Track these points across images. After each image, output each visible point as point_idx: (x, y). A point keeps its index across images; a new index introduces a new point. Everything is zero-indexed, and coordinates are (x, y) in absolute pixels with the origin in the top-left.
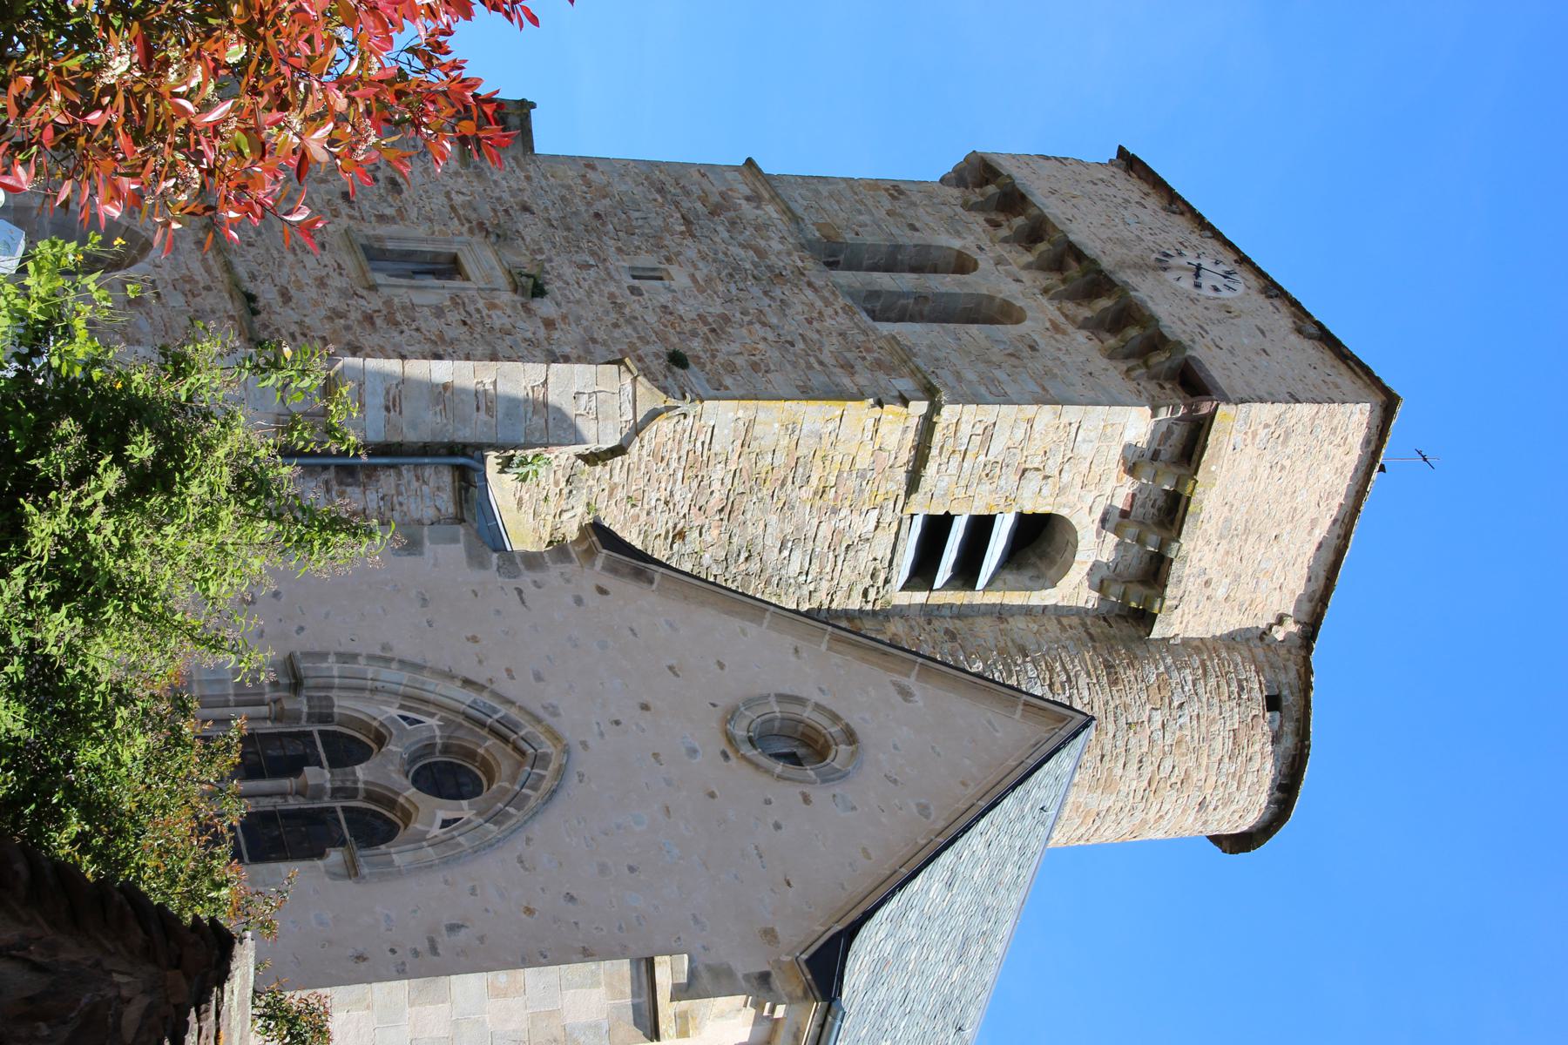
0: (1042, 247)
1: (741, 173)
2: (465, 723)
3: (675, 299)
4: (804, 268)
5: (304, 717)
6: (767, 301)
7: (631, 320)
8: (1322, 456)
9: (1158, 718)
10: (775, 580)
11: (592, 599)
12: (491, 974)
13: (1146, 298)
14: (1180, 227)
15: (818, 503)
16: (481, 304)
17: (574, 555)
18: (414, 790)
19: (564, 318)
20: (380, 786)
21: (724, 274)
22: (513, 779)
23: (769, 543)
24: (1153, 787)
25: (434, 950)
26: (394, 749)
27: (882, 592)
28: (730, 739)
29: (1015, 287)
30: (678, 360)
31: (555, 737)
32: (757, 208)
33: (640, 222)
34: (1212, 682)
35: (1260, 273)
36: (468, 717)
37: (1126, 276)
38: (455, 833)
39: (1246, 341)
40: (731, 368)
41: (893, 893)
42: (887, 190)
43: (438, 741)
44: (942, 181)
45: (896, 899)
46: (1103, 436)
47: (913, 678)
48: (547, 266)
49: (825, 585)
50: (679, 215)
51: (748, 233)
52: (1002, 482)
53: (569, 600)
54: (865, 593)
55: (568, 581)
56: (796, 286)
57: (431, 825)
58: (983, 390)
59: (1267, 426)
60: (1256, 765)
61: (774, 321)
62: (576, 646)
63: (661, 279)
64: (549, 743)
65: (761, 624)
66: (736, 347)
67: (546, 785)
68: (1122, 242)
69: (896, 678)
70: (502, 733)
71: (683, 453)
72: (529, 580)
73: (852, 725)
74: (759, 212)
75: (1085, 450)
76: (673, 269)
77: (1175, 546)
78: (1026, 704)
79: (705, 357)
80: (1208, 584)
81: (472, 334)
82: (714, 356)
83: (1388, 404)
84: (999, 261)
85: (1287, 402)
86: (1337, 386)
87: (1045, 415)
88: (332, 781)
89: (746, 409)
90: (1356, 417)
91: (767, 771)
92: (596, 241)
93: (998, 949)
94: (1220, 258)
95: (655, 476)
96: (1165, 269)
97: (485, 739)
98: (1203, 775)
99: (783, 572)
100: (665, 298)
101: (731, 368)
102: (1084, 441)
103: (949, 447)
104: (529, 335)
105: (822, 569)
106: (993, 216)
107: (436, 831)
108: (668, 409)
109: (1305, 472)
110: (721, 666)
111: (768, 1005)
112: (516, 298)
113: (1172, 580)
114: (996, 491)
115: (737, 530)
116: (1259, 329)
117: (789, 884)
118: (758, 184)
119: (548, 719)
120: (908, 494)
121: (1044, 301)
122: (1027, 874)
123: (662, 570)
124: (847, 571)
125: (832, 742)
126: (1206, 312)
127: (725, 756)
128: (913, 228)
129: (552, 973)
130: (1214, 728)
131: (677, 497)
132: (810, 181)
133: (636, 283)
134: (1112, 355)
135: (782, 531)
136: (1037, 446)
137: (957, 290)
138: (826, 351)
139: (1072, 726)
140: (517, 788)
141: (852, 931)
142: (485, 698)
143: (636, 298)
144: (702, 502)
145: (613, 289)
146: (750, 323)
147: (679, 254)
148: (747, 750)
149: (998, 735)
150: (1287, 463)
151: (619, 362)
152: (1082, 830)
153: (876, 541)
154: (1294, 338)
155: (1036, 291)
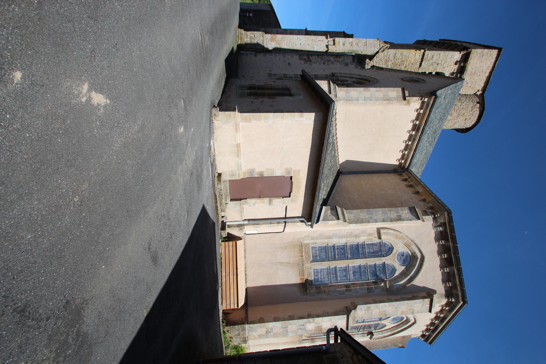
8: (488, 60)
12: (376, 88)
24: (459, 115)
34: (468, 99)
46: (451, 57)
59: (480, 54)
60: (475, 112)
75: (448, 60)
80: (467, 83)
98: (466, 114)
111: (423, 98)
114: (433, 68)
120: (419, 67)
129: (387, 89)
130: (469, 106)
136: (440, 59)
150: (482, 61)
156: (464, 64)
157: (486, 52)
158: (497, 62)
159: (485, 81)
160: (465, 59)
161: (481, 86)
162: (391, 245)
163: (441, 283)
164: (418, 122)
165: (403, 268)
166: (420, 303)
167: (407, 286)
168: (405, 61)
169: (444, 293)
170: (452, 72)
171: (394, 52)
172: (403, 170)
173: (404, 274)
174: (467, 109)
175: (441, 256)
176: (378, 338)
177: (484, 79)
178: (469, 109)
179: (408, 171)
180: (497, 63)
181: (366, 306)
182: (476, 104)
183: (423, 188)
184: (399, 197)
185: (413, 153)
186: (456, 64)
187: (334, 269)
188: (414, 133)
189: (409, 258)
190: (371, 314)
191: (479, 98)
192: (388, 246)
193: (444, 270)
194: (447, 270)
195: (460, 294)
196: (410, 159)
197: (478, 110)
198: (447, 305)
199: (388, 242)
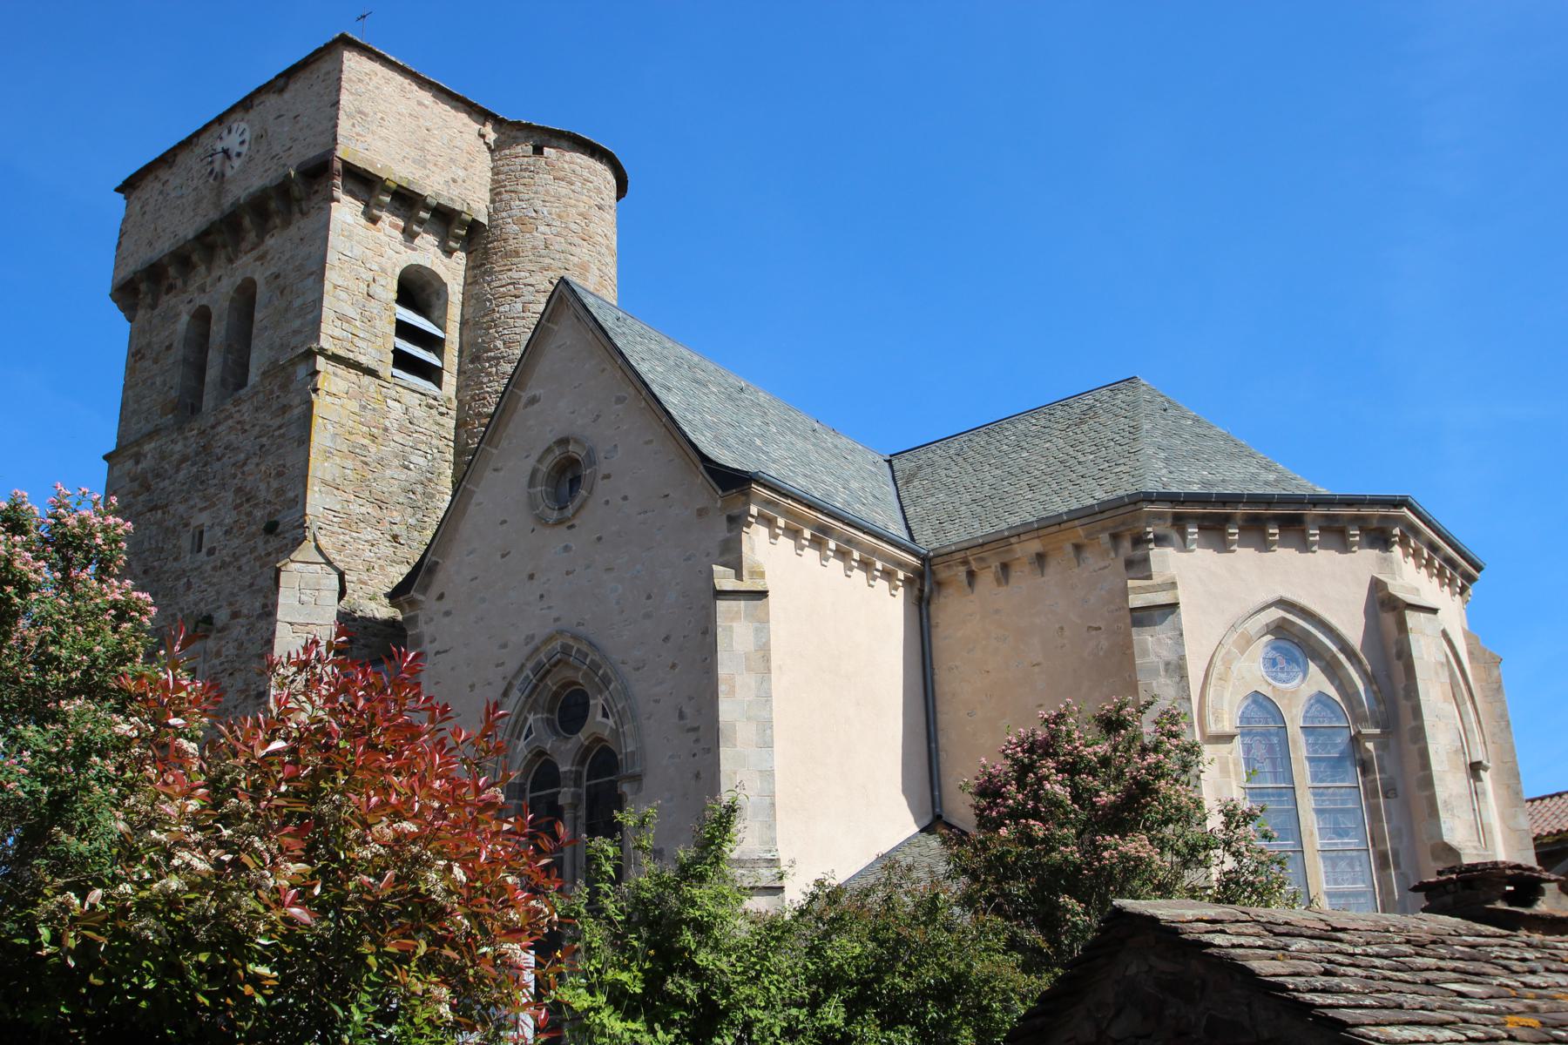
0: (195, 258)
1: (115, 465)
2: (534, 697)
3: (220, 524)
4: (199, 429)
5: (520, 802)
6: (225, 459)
7: (236, 558)
9: (542, 228)
10: (429, 475)
11: (446, 604)
12: (721, 695)
13: (247, 192)
14: (189, 160)
15: (380, 440)
16: (217, 662)
17: (412, 614)
18: (580, 734)
19: (231, 604)
20: (576, 755)
21: (200, 487)
22: (577, 669)
23: (404, 477)
24: (587, 238)
25: (695, 729)
26: (549, 745)
27: (442, 403)
28: (559, 522)
29: (225, 281)
30: (271, 528)
31: (550, 639)
32: (145, 457)
33: (153, 542)
34: (520, 188)
35: (233, 110)
36: (530, 695)
37: (227, 201)
38: (615, 710)
39: (286, 129)
40: (280, 492)
41: (679, 428)
42: (136, 361)
43: (545, 715)
44: (130, 321)
45: (684, 428)
46: (349, 237)
47: (523, 394)
48: (186, 612)
49: (435, 442)
50: (148, 514)
51: (167, 466)
52: (375, 311)
53: (446, 620)
54: (442, 414)
55: (432, 620)
56: (214, 436)
57: (606, 725)
58: (310, 317)
59: (353, 125)
60: (578, 168)
61: (242, 456)
62: (482, 619)
63: (201, 533)
64: (554, 643)
65: (474, 492)
66: (263, 486)
67: (585, 648)
68: (198, 202)
69: (521, 405)
70: (542, 672)
71: (340, 530)
72: (429, 646)
73: (554, 440)
74: (149, 456)
75: (358, 251)
76: (194, 523)
77: (429, 200)
78: (548, 320)
79: (269, 509)
80: (454, 181)
81: (241, 670)
82: (269, 502)
83: (346, 42)
84: (202, 289)
85: (338, 109)
86: (328, 73)
87: (332, 276)
88: (569, 787)
89: (314, 485)
90: (353, 63)
91: (585, 500)
92: (167, 575)
93: (696, 359)
94: (216, 135)
95: (354, 552)
96: (223, 175)
97: (546, 685)
98: (582, 204)
99: (424, 469)
100: (219, 532)
101: (280, 492)
102: (351, 251)
103: (349, 346)
104: (244, 630)
105: (423, 442)
106: (164, 288)
107: (611, 722)
108: (315, 540)
109: (385, 104)
110: (504, 522)
112: (212, 636)
113: (450, 205)
115: (395, 499)
116: (276, 118)
117: (667, 496)
118: (125, 454)
119: (537, 641)
120: (378, 377)
121: (238, 263)
122: (654, 334)
123: (429, 555)
124: (426, 425)
125: (565, 455)
126: (261, 152)
127: (572, 527)
128: (169, 347)
129: (722, 655)
131: (370, 538)
132: (1399, 666)
133: (204, 550)
134: (287, 223)
135: (397, 467)
136: (352, 284)
137: (224, 323)
138: (271, 423)
139: (567, 293)
140: (585, 667)
141: (705, 459)
142: (517, 683)
143: (217, 552)
144: (374, 521)
145: (209, 567)
146: (243, 473)
147: (182, 517)
148: (569, 511)
149: (568, 343)
151: (278, 571)
152: (610, 289)
153: (408, 403)
154: (287, 95)
155: (229, 267)
156: (387, 192)
157: (351, 98)
158: (389, 56)
159: (448, 108)
160: (364, 183)
161: (464, 124)
162: (1246, 698)
163: (1349, 555)
164: (807, 533)
165: (1313, 667)
166: (1418, 641)
167: (1369, 668)
168: (352, 438)
169: (1377, 551)
170: (401, 236)
171: (316, 489)
172: (927, 573)
173: (1332, 669)
174: (563, 200)
175: (1274, 543)
176: (1485, 743)
177: (444, 110)
178: (563, 191)
179: (935, 557)
180: (393, 59)
181: (1443, 815)
182: (542, 162)
183: (1023, 537)
184: (1062, 628)
185: (884, 545)
186: (374, 220)
187: (1334, 901)
188: (832, 544)
189: (1281, 643)
190: (1461, 797)
191: (516, 141)
192: (1250, 708)
193: (1314, 543)
194: (1314, 534)
195: (1383, 512)
196: (898, 552)
197: (568, 156)
198: (1404, 542)
199: (1239, 707)
